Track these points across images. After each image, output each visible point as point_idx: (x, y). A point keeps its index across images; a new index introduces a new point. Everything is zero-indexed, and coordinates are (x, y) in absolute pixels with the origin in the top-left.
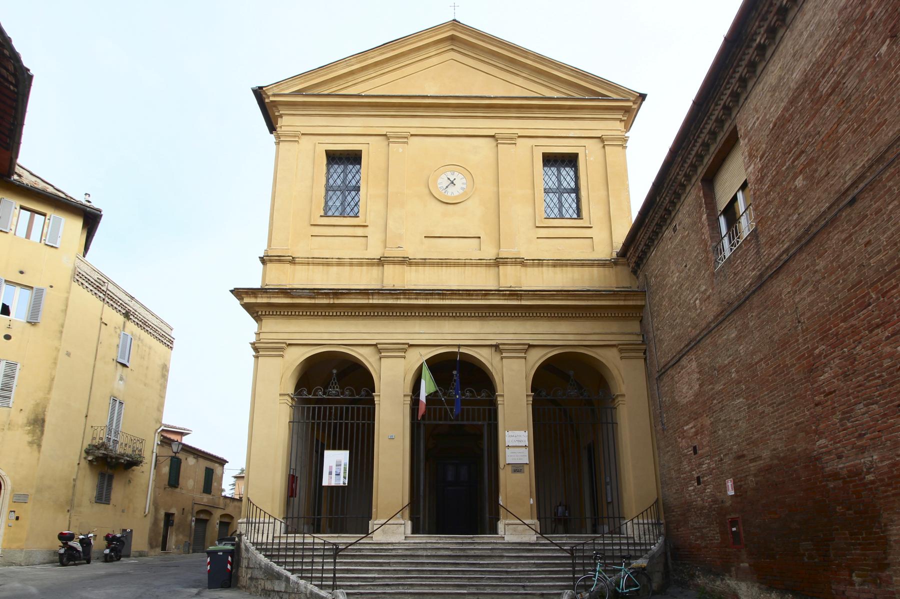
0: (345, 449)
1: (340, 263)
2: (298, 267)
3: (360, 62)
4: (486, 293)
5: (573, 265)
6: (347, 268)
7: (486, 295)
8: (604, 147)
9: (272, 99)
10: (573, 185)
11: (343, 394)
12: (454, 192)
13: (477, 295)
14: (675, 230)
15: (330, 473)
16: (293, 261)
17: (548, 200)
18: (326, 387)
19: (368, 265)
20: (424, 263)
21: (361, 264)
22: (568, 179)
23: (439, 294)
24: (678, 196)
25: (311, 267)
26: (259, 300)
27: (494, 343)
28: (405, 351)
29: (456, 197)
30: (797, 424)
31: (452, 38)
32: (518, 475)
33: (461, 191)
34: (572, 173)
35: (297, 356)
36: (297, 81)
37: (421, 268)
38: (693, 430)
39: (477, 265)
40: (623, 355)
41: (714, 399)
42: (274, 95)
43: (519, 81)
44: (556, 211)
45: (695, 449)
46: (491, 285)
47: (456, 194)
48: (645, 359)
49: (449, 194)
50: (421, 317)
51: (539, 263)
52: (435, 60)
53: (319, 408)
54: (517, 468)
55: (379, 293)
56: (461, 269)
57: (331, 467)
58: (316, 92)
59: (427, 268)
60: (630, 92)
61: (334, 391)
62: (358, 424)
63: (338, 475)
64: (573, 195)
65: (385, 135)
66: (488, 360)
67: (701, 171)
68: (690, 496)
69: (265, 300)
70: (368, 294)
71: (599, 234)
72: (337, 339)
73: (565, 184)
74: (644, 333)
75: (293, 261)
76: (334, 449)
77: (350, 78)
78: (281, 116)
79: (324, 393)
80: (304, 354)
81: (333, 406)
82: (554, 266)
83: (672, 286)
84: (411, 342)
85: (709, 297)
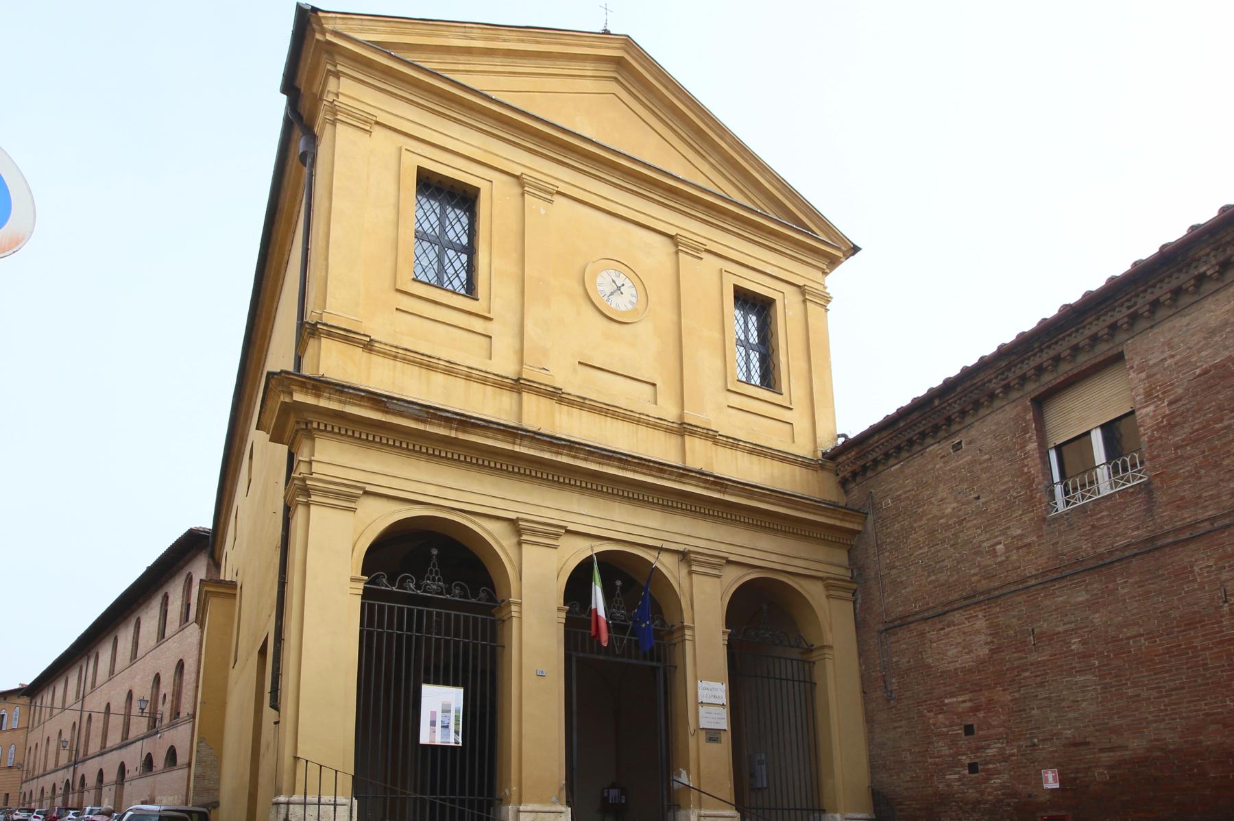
0: (455, 685)
1: (450, 370)
2: (375, 358)
3: (486, 39)
4: (661, 468)
5: (773, 457)
6: (461, 383)
7: (682, 475)
8: (677, 253)
9: (330, 37)
10: (464, 240)
11: (449, 592)
12: (622, 304)
13: (671, 473)
14: (957, 447)
15: (433, 723)
16: (369, 346)
17: (419, 251)
18: (420, 577)
19: (496, 385)
20: (582, 404)
21: (484, 381)
22: (458, 227)
23: (620, 460)
24: (977, 405)
25: (399, 364)
26: (323, 403)
27: (681, 548)
28: (354, 498)
29: (623, 313)
30: (1208, 715)
31: (619, 62)
32: (714, 745)
33: (630, 307)
34: (465, 220)
35: (378, 517)
36: (380, 26)
37: (575, 411)
38: (968, 704)
39: (654, 426)
40: (831, 592)
41: (1027, 670)
42: (336, 33)
43: (705, 167)
44: (431, 274)
45: (969, 730)
46: (672, 459)
47: (623, 308)
48: (854, 603)
49: (613, 305)
50: (582, 490)
51: (733, 443)
52: (589, 85)
53: (410, 612)
54: (713, 735)
55: (533, 438)
56: (632, 427)
57: (433, 714)
58: (410, 57)
59: (584, 414)
60: (842, 238)
61: (434, 585)
62: (457, 644)
63: (445, 727)
64: (464, 258)
65: (517, 177)
66: (671, 572)
67: (1033, 388)
68: (948, 786)
69: (334, 406)
70: (515, 435)
71: (798, 417)
72: (452, 498)
73: (451, 235)
74: (857, 567)
75: (369, 346)
76: (436, 683)
77: (463, 59)
78: (337, 75)
79: (418, 587)
80: (394, 512)
81: (435, 610)
82: (751, 452)
83: (935, 517)
84: (571, 527)
85: (1029, 545)
